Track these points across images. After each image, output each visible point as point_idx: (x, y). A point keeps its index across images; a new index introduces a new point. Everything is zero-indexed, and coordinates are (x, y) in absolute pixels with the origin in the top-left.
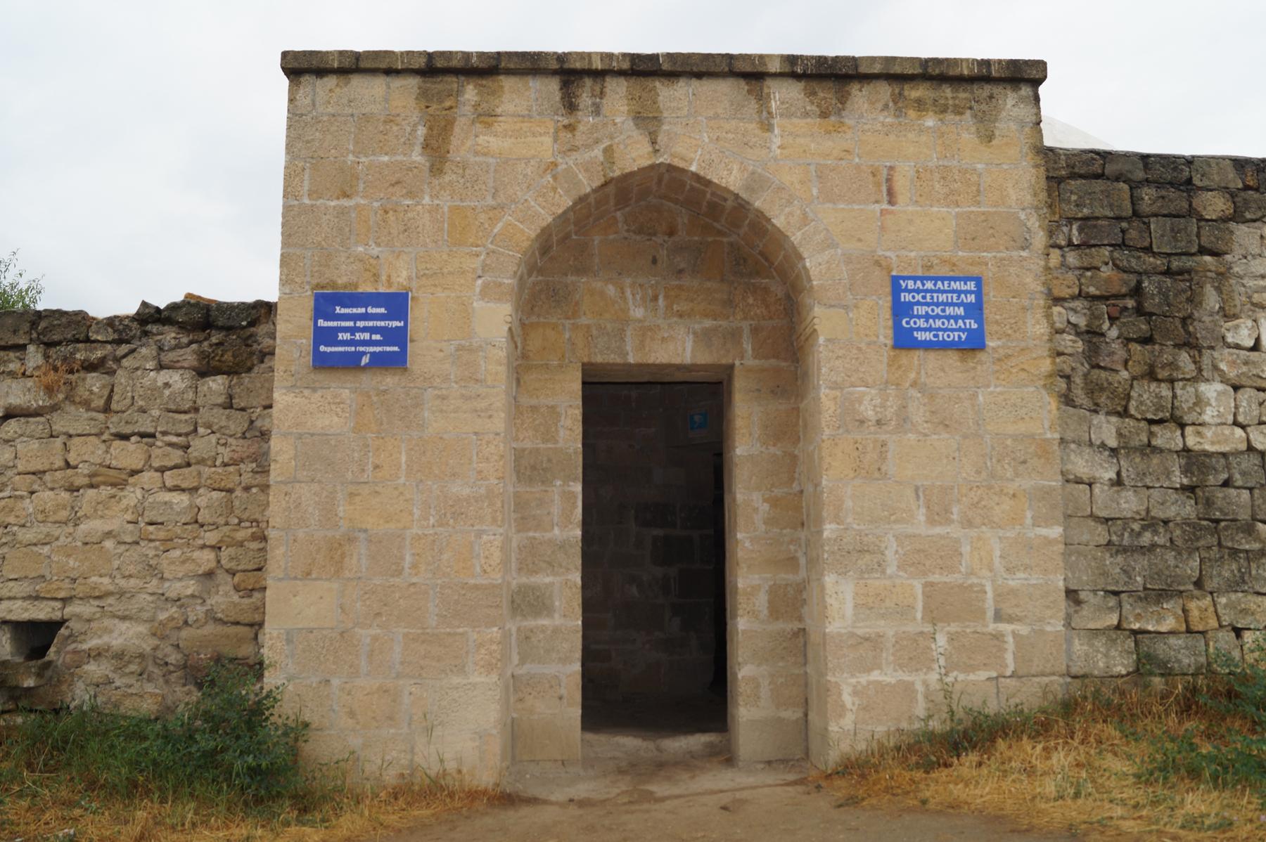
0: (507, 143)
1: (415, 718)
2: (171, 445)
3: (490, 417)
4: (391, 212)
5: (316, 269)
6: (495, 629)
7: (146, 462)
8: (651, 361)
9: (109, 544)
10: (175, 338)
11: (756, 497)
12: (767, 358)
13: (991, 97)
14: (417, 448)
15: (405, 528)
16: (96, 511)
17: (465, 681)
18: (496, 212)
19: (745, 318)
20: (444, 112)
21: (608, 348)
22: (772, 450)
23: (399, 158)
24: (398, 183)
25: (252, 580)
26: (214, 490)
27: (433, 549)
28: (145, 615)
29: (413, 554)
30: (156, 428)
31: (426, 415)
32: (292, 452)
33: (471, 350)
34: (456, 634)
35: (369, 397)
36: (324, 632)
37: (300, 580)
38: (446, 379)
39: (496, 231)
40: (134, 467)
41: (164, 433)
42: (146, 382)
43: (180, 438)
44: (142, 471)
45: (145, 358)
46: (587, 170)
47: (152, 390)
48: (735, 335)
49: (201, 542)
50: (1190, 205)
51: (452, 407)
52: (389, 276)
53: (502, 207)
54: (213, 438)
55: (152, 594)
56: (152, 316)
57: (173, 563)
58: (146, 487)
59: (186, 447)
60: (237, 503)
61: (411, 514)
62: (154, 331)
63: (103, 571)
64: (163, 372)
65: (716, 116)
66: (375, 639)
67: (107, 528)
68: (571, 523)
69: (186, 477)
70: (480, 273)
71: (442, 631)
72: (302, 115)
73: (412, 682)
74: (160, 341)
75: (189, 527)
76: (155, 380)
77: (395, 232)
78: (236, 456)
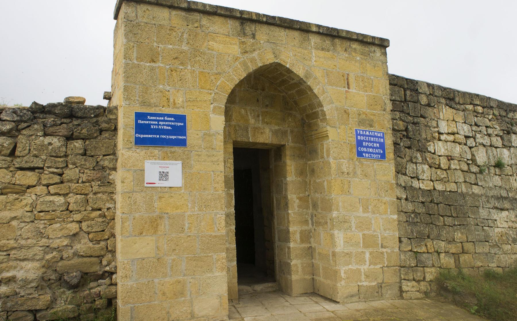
0: (221, 46)
1: (193, 292)
2: (53, 173)
3: (218, 164)
4: (174, 71)
5: (141, 94)
6: (224, 253)
7: (38, 181)
8: (258, 142)
9: (14, 223)
10: (53, 121)
11: (294, 196)
12: (296, 143)
13: (374, 51)
14: (189, 177)
15: (184, 212)
16: (5, 207)
17: (213, 275)
18: (218, 75)
19: (288, 127)
20: (195, 29)
21: (242, 135)
22: (299, 179)
23: (177, 47)
24: (176, 58)
25: (100, 236)
26: (77, 194)
27: (197, 221)
28: (38, 257)
29: (189, 223)
30: (44, 165)
31: (192, 163)
32: (132, 178)
33: (210, 135)
34: (208, 256)
35: (167, 154)
36: (150, 259)
37: (138, 236)
38: (200, 147)
39: (218, 84)
40: (30, 184)
41: (48, 167)
42: (38, 142)
43: (58, 170)
44: (34, 186)
45: (37, 130)
46: (251, 62)
47: (42, 146)
48: (284, 133)
49: (71, 219)
50: (418, 99)
51: (203, 159)
52: (174, 100)
53: (219, 74)
54: (77, 170)
55: (41, 246)
56: (40, 109)
57: (55, 230)
58: (38, 194)
59: (61, 175)
60: (90, 200)
61: (187, 206)
62: (41, 117)
63: (10, 237)
64: (47, 138)
65: (294, 45)
66: (174, 260)
67: (13, 215)
68: (231, 206)
69: (63, 188)
70: (212, 102)
71: (202, 255)
72: (131, 21)
73: (191, 277)
74: (44, 122)
75: (65, 213)
76: (43, 141)
77: (176, 80)
78: (90, 178)
